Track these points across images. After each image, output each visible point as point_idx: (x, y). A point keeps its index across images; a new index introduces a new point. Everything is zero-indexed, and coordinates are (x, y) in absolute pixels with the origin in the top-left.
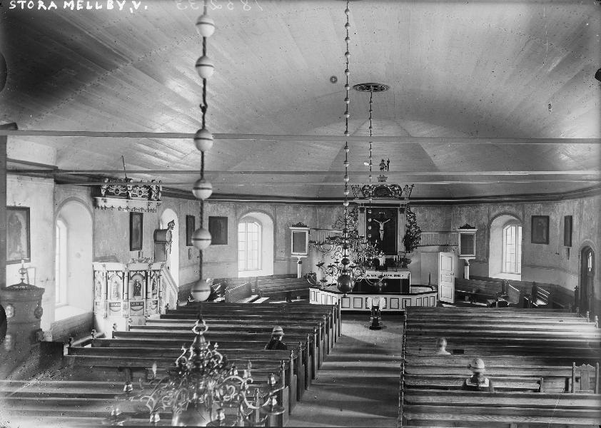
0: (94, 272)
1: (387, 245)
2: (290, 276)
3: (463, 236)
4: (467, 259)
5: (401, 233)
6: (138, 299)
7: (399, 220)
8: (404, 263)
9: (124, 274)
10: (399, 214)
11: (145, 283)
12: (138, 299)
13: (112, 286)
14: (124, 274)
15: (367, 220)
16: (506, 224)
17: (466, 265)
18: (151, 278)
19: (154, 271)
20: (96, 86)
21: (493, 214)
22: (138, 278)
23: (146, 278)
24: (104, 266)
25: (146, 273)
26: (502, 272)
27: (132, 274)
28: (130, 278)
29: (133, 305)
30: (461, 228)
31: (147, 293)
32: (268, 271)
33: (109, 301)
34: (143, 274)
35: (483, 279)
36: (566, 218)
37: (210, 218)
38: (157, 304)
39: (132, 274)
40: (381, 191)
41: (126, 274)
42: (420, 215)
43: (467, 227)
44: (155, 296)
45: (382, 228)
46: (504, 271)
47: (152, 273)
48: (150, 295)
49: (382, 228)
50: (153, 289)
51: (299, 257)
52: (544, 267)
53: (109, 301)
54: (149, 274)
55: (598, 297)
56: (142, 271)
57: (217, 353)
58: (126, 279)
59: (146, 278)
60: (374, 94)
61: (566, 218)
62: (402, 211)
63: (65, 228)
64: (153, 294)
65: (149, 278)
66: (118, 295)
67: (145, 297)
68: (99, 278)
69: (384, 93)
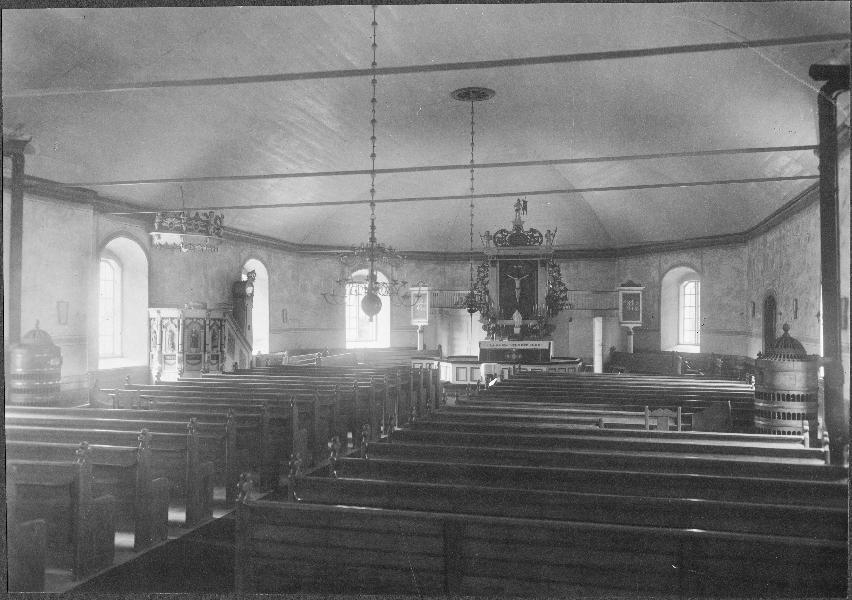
0: (150, 320)
1: (526, 306)
2: (411, 348)
3: (627, 297)
4: (631, 326)
5: (543, 291)
7: (541, 276)
8: (546, 331)
10: (539, 270)
13: (167, 335)
15: (720, 356)
16: (682, 280)
17: (630, 333)
19: (214, 320)
21: (666, 266)
24: (159, 312)
26: (678, 344)
27: (189, 321)
30: (623, 286)
31: (205, 344)
32: (388, 345)
34: (202, 323)
35: (655, 352)
38: (217, 359)
40: (518, 237)
42: (567, 272)
43: (631, 284)
45: (517, 285)
46: (681, 341)
48: (209, 348)
49: (517, 285)
51: (420, 325)
54: (208, 323)
55: (847, 396)
60: (477, 104)
62: (544, 264)
63: (120, 269)
65: (207, 327)
66: (173, 347)
68: (156, 327)
69: (492, 100)
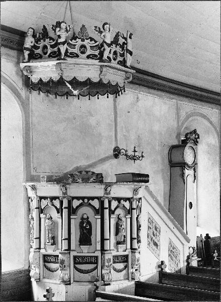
6: (85, 251)
9: (61, 203)
11: (99, 221)
12: (85, 251)
14: (61, 203)
18: (112, 212)
19: (119, 200)
20: (162, 170)
22: (86, 211)
23: (100, 212)
25: (102, 203)
27: (76, 203)
28: (72, 211)
29: (78, 260)
31: (103, 240)
33: (43, 251)
34: (96, 203)
36: (147, 176)
37: (136, 295)
38: (127, 261)
39: (76, 203)
41: (65, 204)
44: (122, 247)
47: (114, 204)
48: (110, 244)
50: (117, 233)
52: (195, 172)
53: (43, 251)
54: (106, 205)
56: (93, 198)
57: (124, 116)
58: (65, 212)
59: (100, 212)
61: (147, 176)
64: (118, 243)
65: (107, 212)
67: (99, 247)
